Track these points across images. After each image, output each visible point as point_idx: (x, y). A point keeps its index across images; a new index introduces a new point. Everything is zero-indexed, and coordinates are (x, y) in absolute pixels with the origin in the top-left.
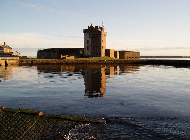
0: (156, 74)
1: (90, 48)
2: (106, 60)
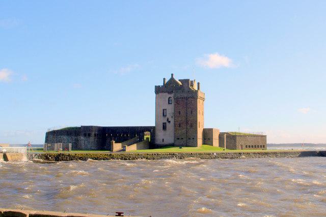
0: (285, 200)
1: (170, 127)
2: (215, 154)
